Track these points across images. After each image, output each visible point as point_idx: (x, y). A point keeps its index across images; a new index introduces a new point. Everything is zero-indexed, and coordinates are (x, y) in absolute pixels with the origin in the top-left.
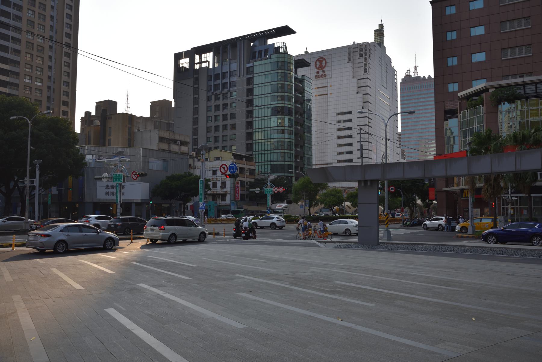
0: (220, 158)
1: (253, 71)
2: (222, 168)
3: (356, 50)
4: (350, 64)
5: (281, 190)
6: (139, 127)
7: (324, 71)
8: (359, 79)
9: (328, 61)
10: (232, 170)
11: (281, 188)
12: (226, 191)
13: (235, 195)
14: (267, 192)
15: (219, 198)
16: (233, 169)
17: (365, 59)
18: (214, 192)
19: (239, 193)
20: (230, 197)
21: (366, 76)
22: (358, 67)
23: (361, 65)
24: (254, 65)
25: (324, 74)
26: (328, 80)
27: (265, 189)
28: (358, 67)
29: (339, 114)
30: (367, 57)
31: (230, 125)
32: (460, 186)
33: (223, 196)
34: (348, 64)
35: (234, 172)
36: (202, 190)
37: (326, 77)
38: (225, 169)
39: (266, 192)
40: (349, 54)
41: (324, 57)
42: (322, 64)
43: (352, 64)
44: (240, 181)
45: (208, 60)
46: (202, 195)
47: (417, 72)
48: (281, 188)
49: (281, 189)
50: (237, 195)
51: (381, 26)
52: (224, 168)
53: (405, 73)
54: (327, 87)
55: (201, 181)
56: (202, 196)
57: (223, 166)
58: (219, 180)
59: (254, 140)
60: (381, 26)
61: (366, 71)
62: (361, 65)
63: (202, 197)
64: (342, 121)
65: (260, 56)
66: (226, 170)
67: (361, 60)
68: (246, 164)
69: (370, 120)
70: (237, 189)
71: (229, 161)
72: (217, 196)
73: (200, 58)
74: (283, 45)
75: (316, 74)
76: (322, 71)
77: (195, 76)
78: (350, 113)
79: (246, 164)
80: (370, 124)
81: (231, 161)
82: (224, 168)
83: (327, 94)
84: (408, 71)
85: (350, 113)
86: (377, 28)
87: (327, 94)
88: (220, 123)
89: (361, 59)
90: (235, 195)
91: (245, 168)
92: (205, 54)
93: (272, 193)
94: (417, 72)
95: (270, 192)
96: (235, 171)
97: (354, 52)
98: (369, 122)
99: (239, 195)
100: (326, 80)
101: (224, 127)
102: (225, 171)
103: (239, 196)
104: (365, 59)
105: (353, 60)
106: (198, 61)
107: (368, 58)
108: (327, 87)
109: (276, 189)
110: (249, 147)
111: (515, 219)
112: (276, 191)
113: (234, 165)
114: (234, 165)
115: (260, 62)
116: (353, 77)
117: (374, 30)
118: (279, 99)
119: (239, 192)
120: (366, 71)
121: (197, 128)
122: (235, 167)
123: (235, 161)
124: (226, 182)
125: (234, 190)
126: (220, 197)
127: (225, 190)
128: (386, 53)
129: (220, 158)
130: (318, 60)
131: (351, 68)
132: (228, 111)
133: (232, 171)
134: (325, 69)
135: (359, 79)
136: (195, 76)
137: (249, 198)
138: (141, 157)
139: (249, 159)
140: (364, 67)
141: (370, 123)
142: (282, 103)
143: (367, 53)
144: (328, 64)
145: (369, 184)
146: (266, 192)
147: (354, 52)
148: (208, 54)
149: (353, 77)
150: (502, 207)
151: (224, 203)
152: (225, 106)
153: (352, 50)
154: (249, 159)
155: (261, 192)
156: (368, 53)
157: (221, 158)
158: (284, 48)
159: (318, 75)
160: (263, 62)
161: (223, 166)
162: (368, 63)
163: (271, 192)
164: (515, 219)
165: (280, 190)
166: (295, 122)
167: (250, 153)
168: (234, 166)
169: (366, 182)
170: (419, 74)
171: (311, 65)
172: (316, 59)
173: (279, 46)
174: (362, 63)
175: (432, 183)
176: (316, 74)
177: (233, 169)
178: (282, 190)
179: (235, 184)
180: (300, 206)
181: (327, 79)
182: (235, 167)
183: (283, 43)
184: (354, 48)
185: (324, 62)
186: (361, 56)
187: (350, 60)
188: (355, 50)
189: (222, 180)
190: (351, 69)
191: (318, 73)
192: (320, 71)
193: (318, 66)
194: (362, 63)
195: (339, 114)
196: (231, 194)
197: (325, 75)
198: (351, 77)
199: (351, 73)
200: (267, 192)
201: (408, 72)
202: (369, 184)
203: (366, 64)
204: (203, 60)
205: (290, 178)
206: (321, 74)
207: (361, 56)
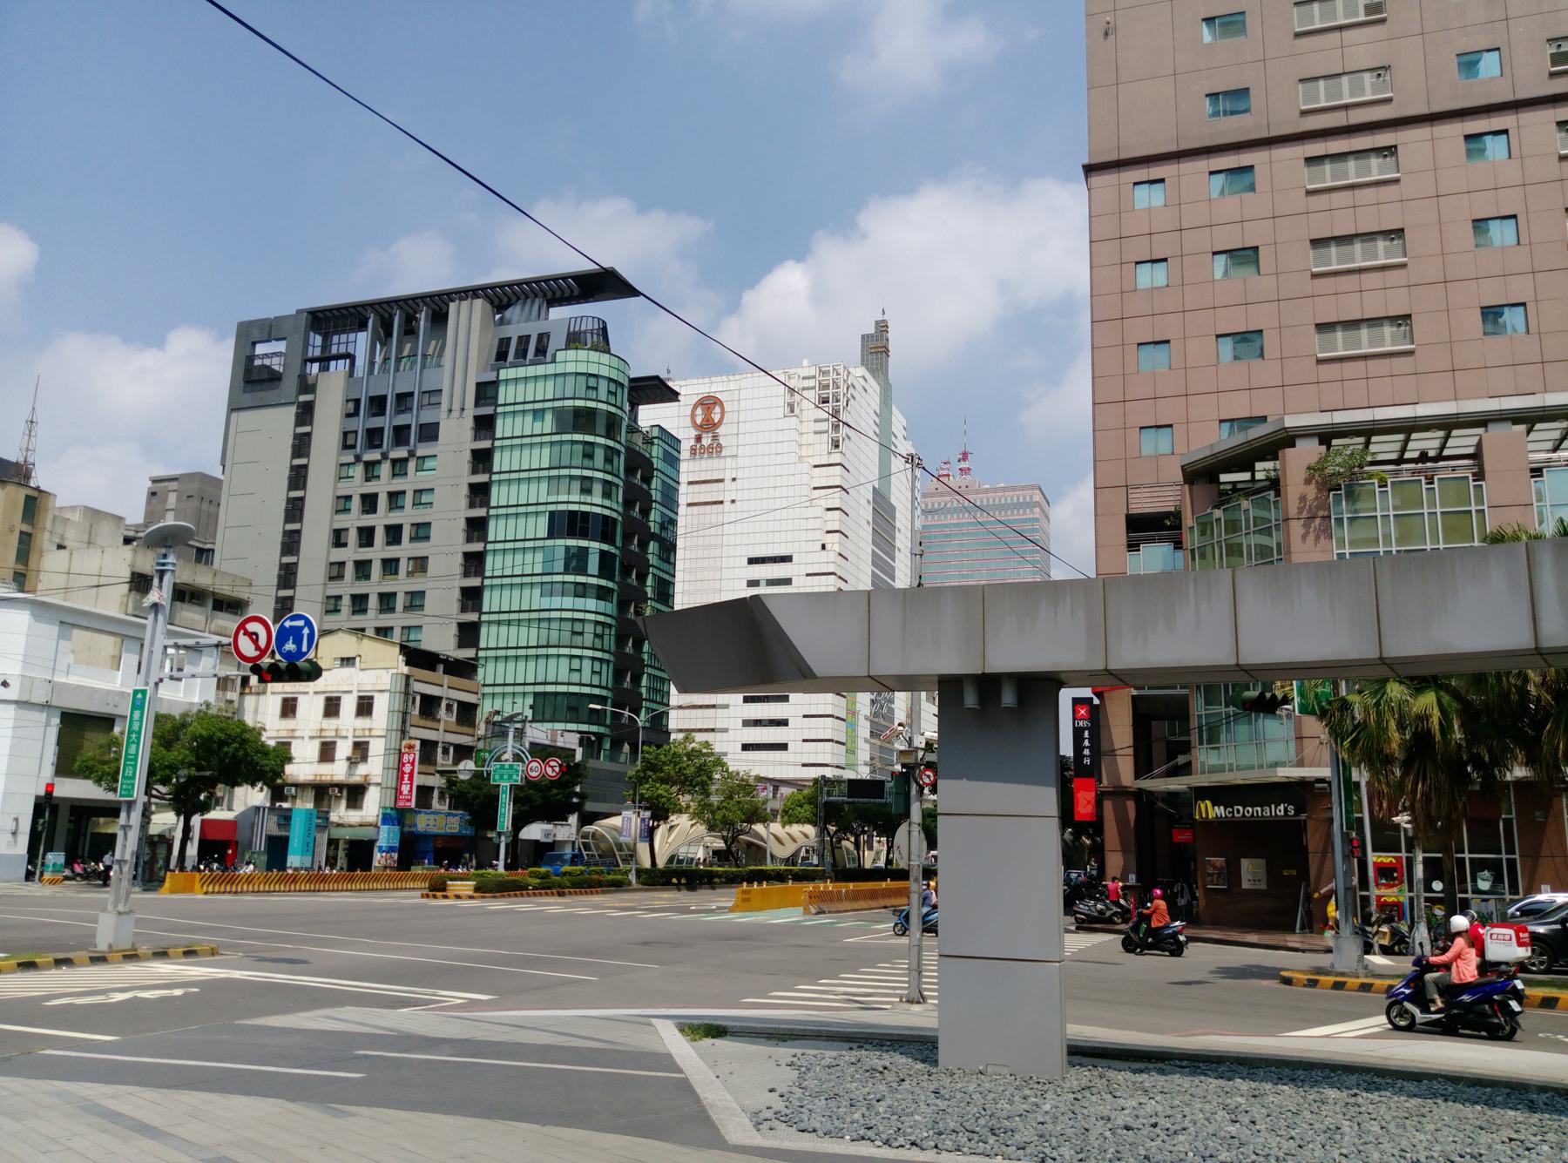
0: (354, 658)
1: (496, 397)
2: (247, 633)
3: (811, 383)
5: (553, 770)
6: (62, 537)
7: (715, 437)
10: (290, 646)
11: (552, 763)
12: (366, 776)
13: (398, 791)
14: (501, 777)
15: (338, 798)
16: (298, 642)
18: (323, 778)
19: (411, 784)
20: (378, 795)
21: (836, 458)
23: (824, 426)
24: (500, 378)
27: (494, 766)
29: (752, 561)
31: (409, 559)
32: (1190, 774)
33: (355, 793)
35: (300, 654)
36: (138, 739)
38: (255, 642)
39: (497, 777)
41: (718, 395)
44: (419, 742)
45: (351, 350)
46: (136, 761)
48: (552, 763)
49: (552, 767)
50: (405, 789)
51: (882, 327)
52: (254, 637)
54: (722, 481)
55: (139, 696)
56: (135, 767)
57: (252, 627)
58: (344, 734)
59: (485, 613)
60: (882, 327)
62: (824, 426)
63: (134, 774)
64: (763, 583)
65: (522, 353)
66: (262, 642)
68: (445, 687)
70: (407, 769)
71: (384, 672)
72: (334, 791)
73: (326, 346)
74: (596, 327)
76: (710, 435)
77: (303, 398)
78: (786, 559)
79: (445, 687)
81: (395, 671)
82: (254, 637)
83: (722, 502)
85: (786, 559)
86: (872, 330)
87: (722, 502)
88: (379, 551)
90: (398, 791)
91: (440, 698)
92: (344, 337)
93: (518, 780)
95: (510, 777)
96: (304, 649)
99: (411, 788)
100: (722, 461)
101: (365, 535)
102: (258, 648)
103: (411, 791)
105: (801, 410)
106: (317, 353)
108: (722, 481)
109: (534, 764)
110: (468, 634)
112: (534, 774)
113: (301, 623)
114: (301, 623)
115: (521, 372)
117: (863, 337)
118: (576, 485)
119: (411, 779)
121: (296, 564)
122: (306, 631)
123: (406, 670)
124: (367, 743)
125: (395, 771)
126: (345, 792)
127: (362, 769)
129: (354, 658)
132: (407, 517)
133: (289, 652)
134: (721, 431)
136: (303, 398)
137: (448, 800)
138: (270, 712)
139: (464, 669)
142: (582, 500)
145: (1008, 698)
146: (497, 777)
148: (352, 336)
150: (1517, 856)
151: (353, 816)
152: (395, 498)
154: (464, 669)
155: (477, 775)
157: (358, 659)
158: (598, 335)
160: (531, 371)
161: (252, 627)
163: (514, 777)
165: (549, 770)
166: (622, 564)
167: (469, 653)
168: (301, 628)
169: (988, 684)
171: (680, 398)
172: (695, 400)
173: (583, 328)
175: (1087, 761)
177: (298, 642)
178: (557, 769)
179: (400, 750)
180: (453, 769)
181: (725, 457)
182: (306, 631)
183: (596, 320)
185: (717, 409)
187: (792, 411)
189: (354, 737)
195: (752, 561)
196: (384, 785)
200: (501, 777)
202: (1008, 698)
204: (334, 350)
205: (593, 738)
206: (706, 441)
207: (824, 402)
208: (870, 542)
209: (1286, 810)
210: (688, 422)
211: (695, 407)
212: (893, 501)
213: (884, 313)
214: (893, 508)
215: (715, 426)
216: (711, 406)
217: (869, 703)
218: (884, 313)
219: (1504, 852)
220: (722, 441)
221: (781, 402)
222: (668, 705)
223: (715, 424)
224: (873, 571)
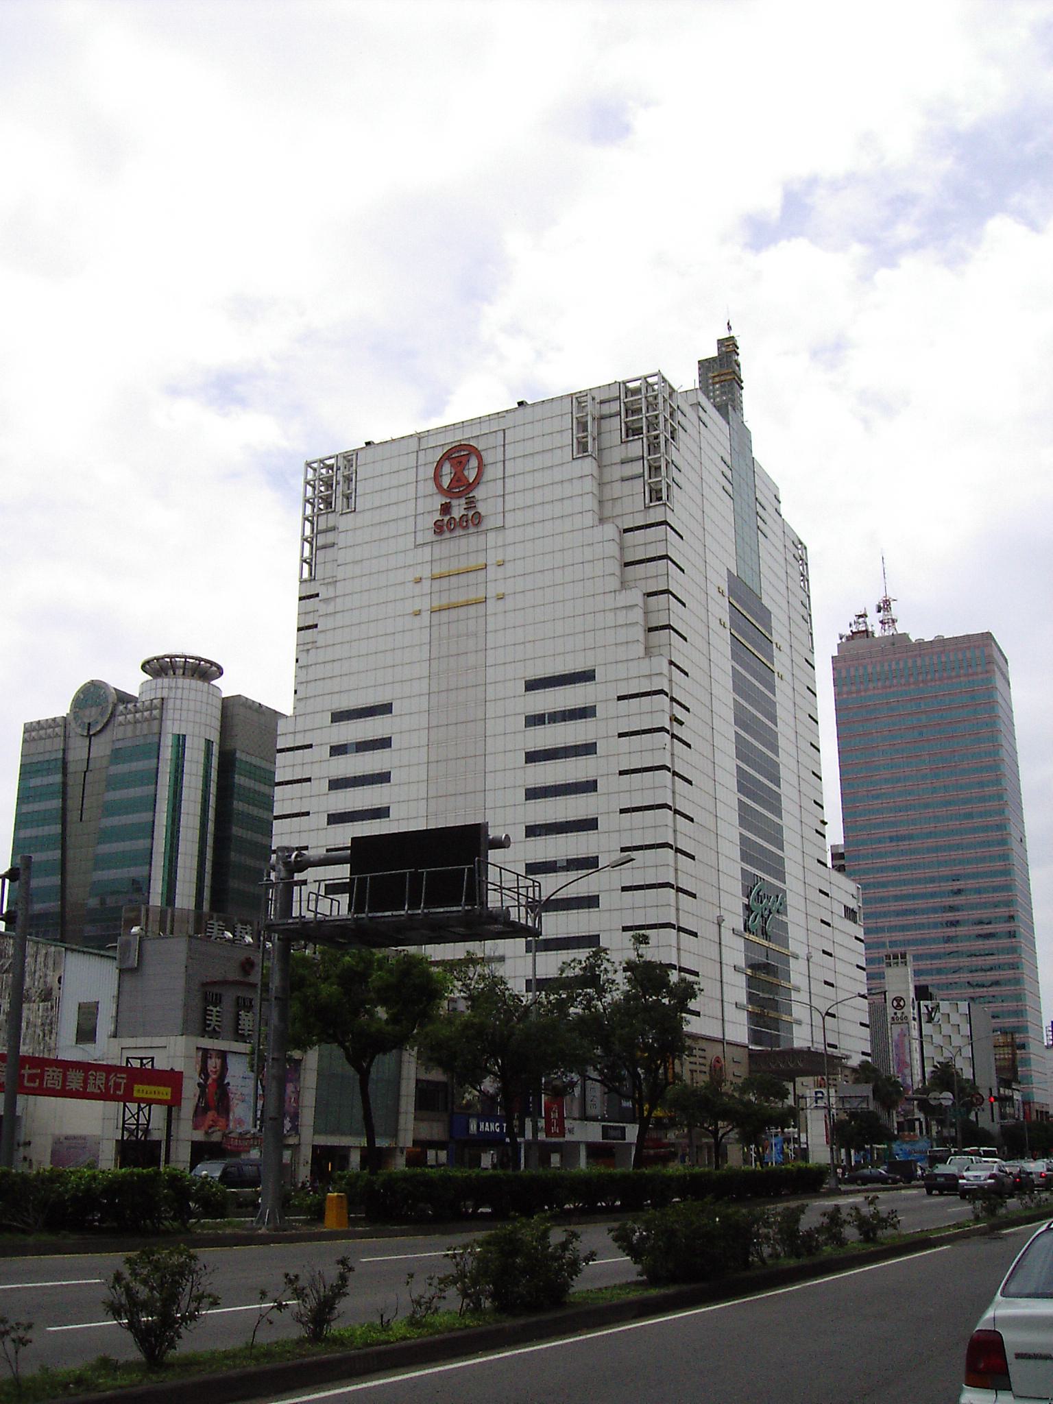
3: (614, 407)
4: (588, 466)
7: (471, 504)
8: (650, 595)
9: (488, 457)
17: (653, 447)
21: (656, 515)
22: (623, 480)
23: (637, 468)
25: (471, 513)
26: (491, 535)
28: (623, 480)
29: (532, 685)
30: (663, 433)
34: (575, 462)
37: (483, 527)
40: (583, 426)
42: (466, 473)
43: (595, 464)
47: (894, 621)
51: (728, 347)
53: (851, 625)
60: (728, 347)
61: (656, 495)
62: (637, 468)
67: (636, 448)
69: (680, 713)
75: (437, 516)
76: (463, 501)
78: (587, 676)
80: (677, 730)
84: (860, 616)
85: (587, 676)
86: (713, 352)
89: (658, 508)
94: (894, 621)
97: (602, 418)
98: (674, 719)
100: (482, 537)
104: (653, 447)
107: (666, 440)
111: (34, 1071)
116: (602, 521)
120: (656, 495)
128: (756, 454)
130: (447, 457)
131: (589, 480)
134: (479, 493)
135: (650, 595)
140: (622, 398)
141: (681, 723)
143: (661, 419)
144: (490, 473)
147: (602, 418)
149: (602, 521)
153: (591, 409)
156: (666, 420)
159: (446, 518)
162: (668, 463)
164: (34, 1071)
170: (900, 628)
172: (439, 454)
174: (637, 459)
176: (437, 516)
184: (602, 402)
185: (474, 462)
186: (633, 431)
188: (607, 409)
190: (590, 485)
191: (446, 509)
192: (455, 502)
193: (446, 482)
194: (637, 459)
195: (532, 685)
197: (478, 519)
198: (589, 519)
199: (590, 503)
201: (861, 620)
203: (655, 469)
206: (457, 512)
208: (730, 685)
209: (949, 1132)
210: (431, 487)
211: (440, 464)
212: (766, 601)
213: (730, 328)
214: (768, 613)
215: (471, 486)
216: (464, 460)
217: (740, 910)
218: (730, 328)
219: (30, 1072)
220: (482, 508)
221: (567, 438)
222: (536, 951)
223: (449, 458)
224: (782, 850)
